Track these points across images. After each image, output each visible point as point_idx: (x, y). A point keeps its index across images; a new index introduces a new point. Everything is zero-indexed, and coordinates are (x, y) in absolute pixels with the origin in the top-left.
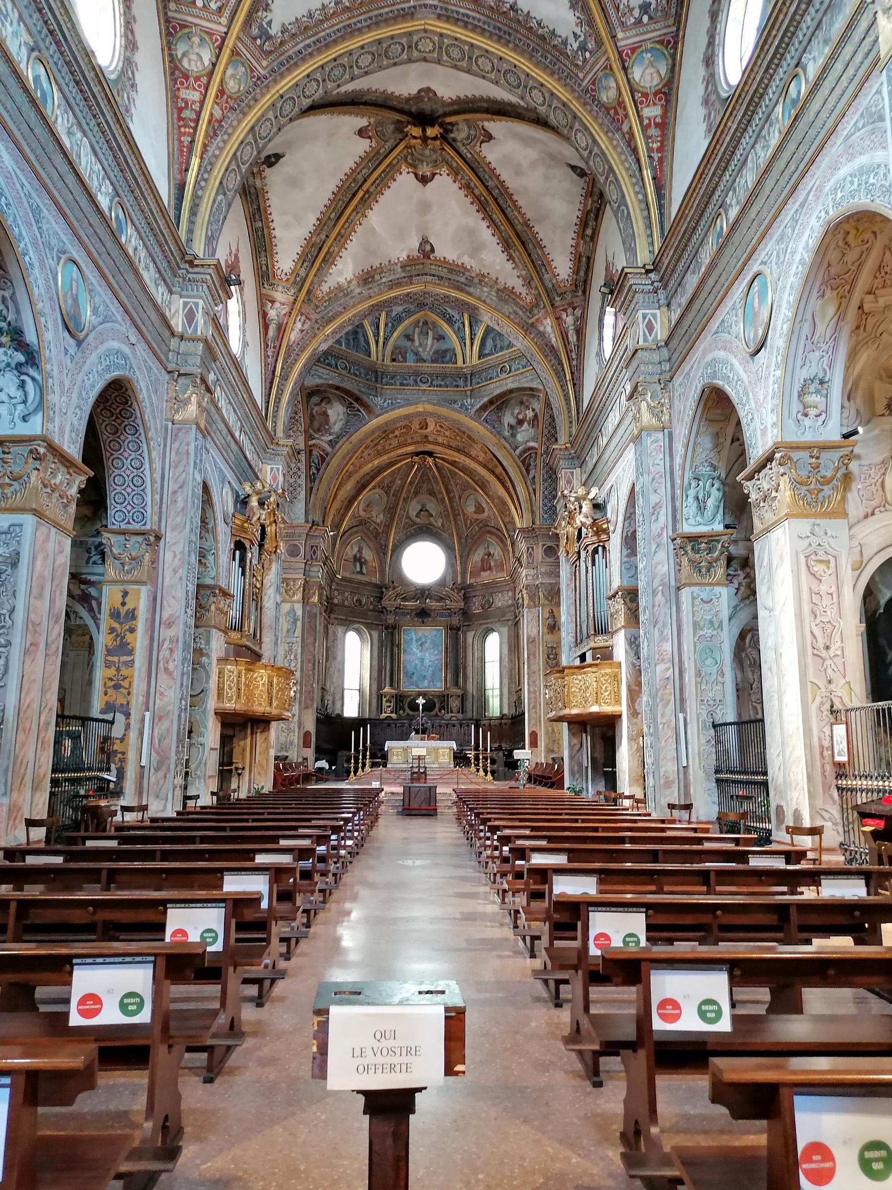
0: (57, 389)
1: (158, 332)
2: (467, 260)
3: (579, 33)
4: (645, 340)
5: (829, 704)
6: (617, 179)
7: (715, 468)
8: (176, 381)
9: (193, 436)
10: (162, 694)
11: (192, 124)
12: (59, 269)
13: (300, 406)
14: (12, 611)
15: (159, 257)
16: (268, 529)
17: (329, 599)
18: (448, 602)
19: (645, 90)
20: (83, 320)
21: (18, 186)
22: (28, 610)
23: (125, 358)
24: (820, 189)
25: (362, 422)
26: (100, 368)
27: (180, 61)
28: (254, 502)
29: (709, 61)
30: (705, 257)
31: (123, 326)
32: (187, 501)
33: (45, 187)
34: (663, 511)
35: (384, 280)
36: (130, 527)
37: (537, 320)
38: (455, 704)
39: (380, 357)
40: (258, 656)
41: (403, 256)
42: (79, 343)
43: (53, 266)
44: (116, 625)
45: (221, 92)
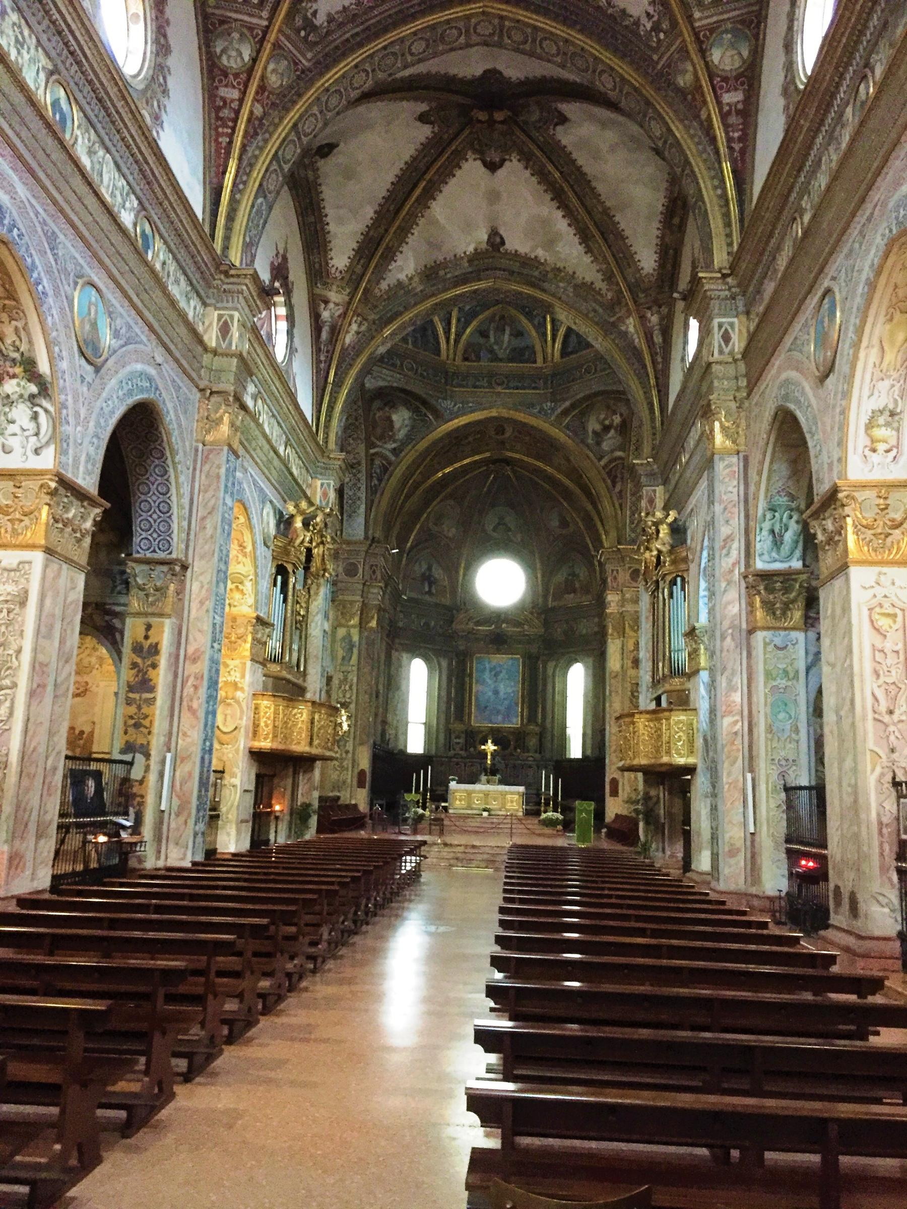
0: (71, 419)
1: (186, 347)
2: (540, 253)
3: (652, 12)
4: (721, 352)
5: (890, 775)
6: (693, 172)
7: (792, 498)
8: (208, 399)
9: (224, 458)
10: (185, 734)
11: (230, 124)
12: (76, 294)
13: (360, 411)
14: (19, 651)
15: (191, 270)
16: (315, 551)
17: (392, 623)
18: (526, 627)
19: (723, 74)
20: (102, 345)
21: (32, 215)
22: (35, 650)
23: (150, 379)
24: (885, 204)
25: (430, 428)
26: (121, 393)
27: (219, 57)
28: (298, 524)
29: (789, 46)
30: (782, 262)
31: (149, 345)
32: (215, 528)
33: (62, 211)
34: (735, 545)
35: (449, 276)
36: (155, 556)
37: (619, 319)
38: (532, 742)
39: (451, 356)
40: (302, 691)
41: (471, 249)
42: (97, 369)
43: (69, 292)
44: (139, 661)
45: (262, 88)
